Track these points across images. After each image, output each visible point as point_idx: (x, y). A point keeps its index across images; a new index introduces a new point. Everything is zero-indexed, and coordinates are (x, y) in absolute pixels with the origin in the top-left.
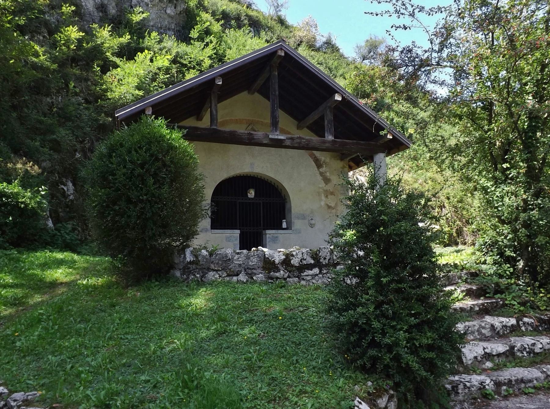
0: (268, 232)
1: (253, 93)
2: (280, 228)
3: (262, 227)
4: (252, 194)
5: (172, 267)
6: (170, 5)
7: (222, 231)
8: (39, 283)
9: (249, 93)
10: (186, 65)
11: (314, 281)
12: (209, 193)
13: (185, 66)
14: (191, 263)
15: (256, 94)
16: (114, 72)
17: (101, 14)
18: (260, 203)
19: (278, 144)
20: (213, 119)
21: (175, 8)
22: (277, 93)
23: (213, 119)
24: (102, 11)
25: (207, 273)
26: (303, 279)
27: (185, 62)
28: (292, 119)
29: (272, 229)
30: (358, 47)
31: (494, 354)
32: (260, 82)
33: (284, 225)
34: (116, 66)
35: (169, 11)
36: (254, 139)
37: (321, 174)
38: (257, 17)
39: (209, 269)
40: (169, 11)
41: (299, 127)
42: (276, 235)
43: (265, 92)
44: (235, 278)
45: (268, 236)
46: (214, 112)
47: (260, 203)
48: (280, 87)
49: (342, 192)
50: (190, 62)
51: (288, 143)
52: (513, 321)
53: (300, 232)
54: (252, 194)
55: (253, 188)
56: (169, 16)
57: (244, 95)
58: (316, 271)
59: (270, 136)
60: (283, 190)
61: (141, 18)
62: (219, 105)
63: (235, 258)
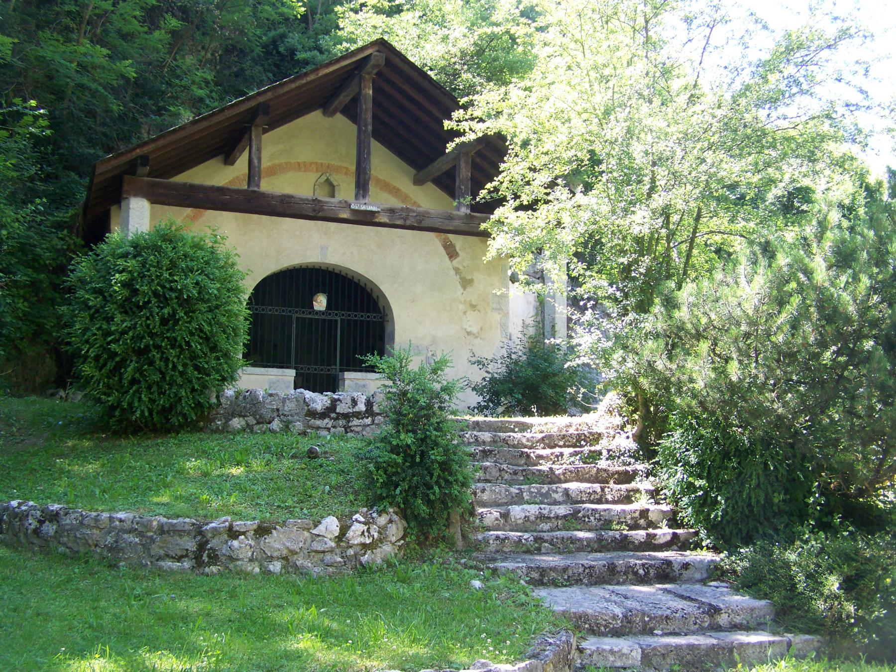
0: (347, 375)
1: (332, 114)
3: (338, 367)
4: (321, 303)
7: (262, 369)
8: (103, 397)
9: (324, 113)
11: (364, 433)
12: (241, 307)
15: (339, 117)
18: (336, 321)
19: (366, 219)
20: (253, 174)
22: (370, 128)
23: (253, 174)
25: (231, 420)
26: (352, 431)
28: (404, 165)
29: (355, 371)
31: (552, 515)
32: (344, 98)
36: (323, 210)
37: (457, 270)
41: (418, 181)
42: (363, 382)
43: (351, 112)
45: (347, 382)
46: (256, 161)
47: (336, 321)
48: (374, 117)
49: (494, 306)
51: (384, 219)
54: (321, 303)
55: (324, 292)
57: (316, 116)
58: (368, 421)
59: (353, 207)
60: (381, 299)
62: (265, 137)
63: (267, 401)
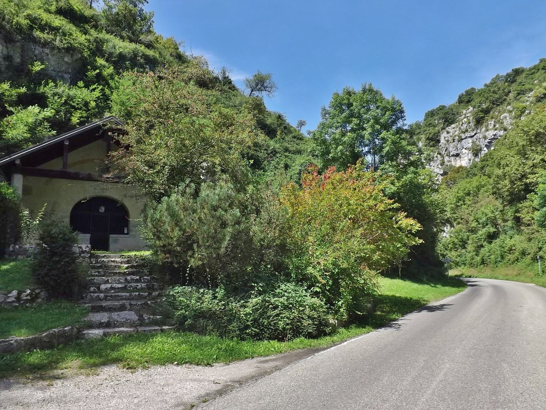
0: (111, 236)
2: (123, 233)
4: (102, 209)
5: (5, 253)
6: (67, 55)
10: (74, 106)
13: (73, 107)
14: (12, 251)
16: (9, 118)
17: (7, 63)
21: (72, 57)
23: (65, 165)
24: (7, 61)
27: (73, 104)
30: (247, 80)
33: (126, 231)
34: (11, 113)
35: (66, 59)
38: (153, 56)
39: (19, 254)
40: (66, 59)
44: (29, 259)
45: (111, 238)
50: (78, 104)
52: (138, 277)
53: (135, 237)
54: (102, 209)
55: (103, 205)
56: (66, 62)
61: (39, 69)
